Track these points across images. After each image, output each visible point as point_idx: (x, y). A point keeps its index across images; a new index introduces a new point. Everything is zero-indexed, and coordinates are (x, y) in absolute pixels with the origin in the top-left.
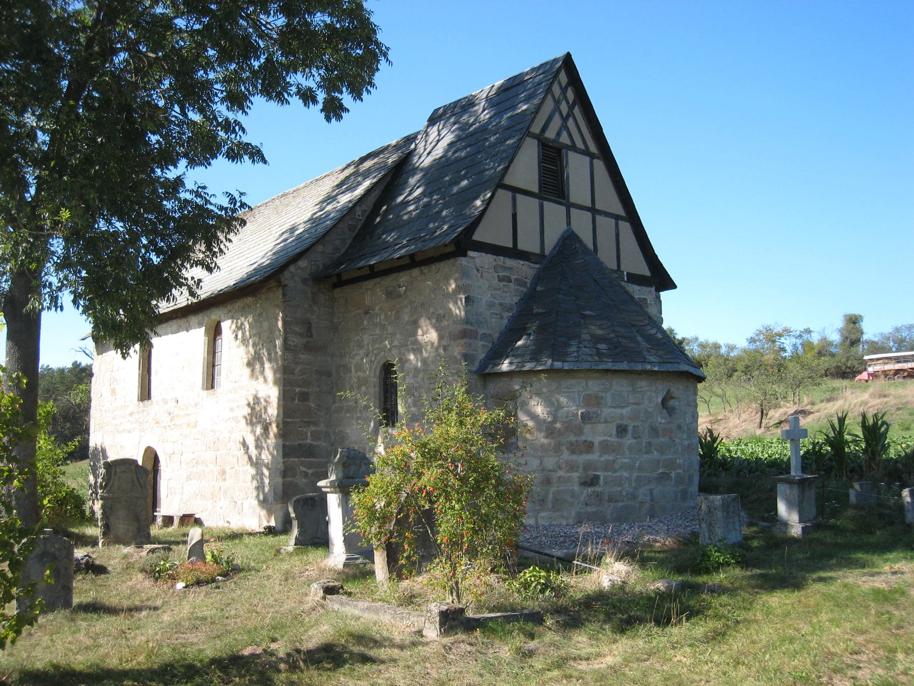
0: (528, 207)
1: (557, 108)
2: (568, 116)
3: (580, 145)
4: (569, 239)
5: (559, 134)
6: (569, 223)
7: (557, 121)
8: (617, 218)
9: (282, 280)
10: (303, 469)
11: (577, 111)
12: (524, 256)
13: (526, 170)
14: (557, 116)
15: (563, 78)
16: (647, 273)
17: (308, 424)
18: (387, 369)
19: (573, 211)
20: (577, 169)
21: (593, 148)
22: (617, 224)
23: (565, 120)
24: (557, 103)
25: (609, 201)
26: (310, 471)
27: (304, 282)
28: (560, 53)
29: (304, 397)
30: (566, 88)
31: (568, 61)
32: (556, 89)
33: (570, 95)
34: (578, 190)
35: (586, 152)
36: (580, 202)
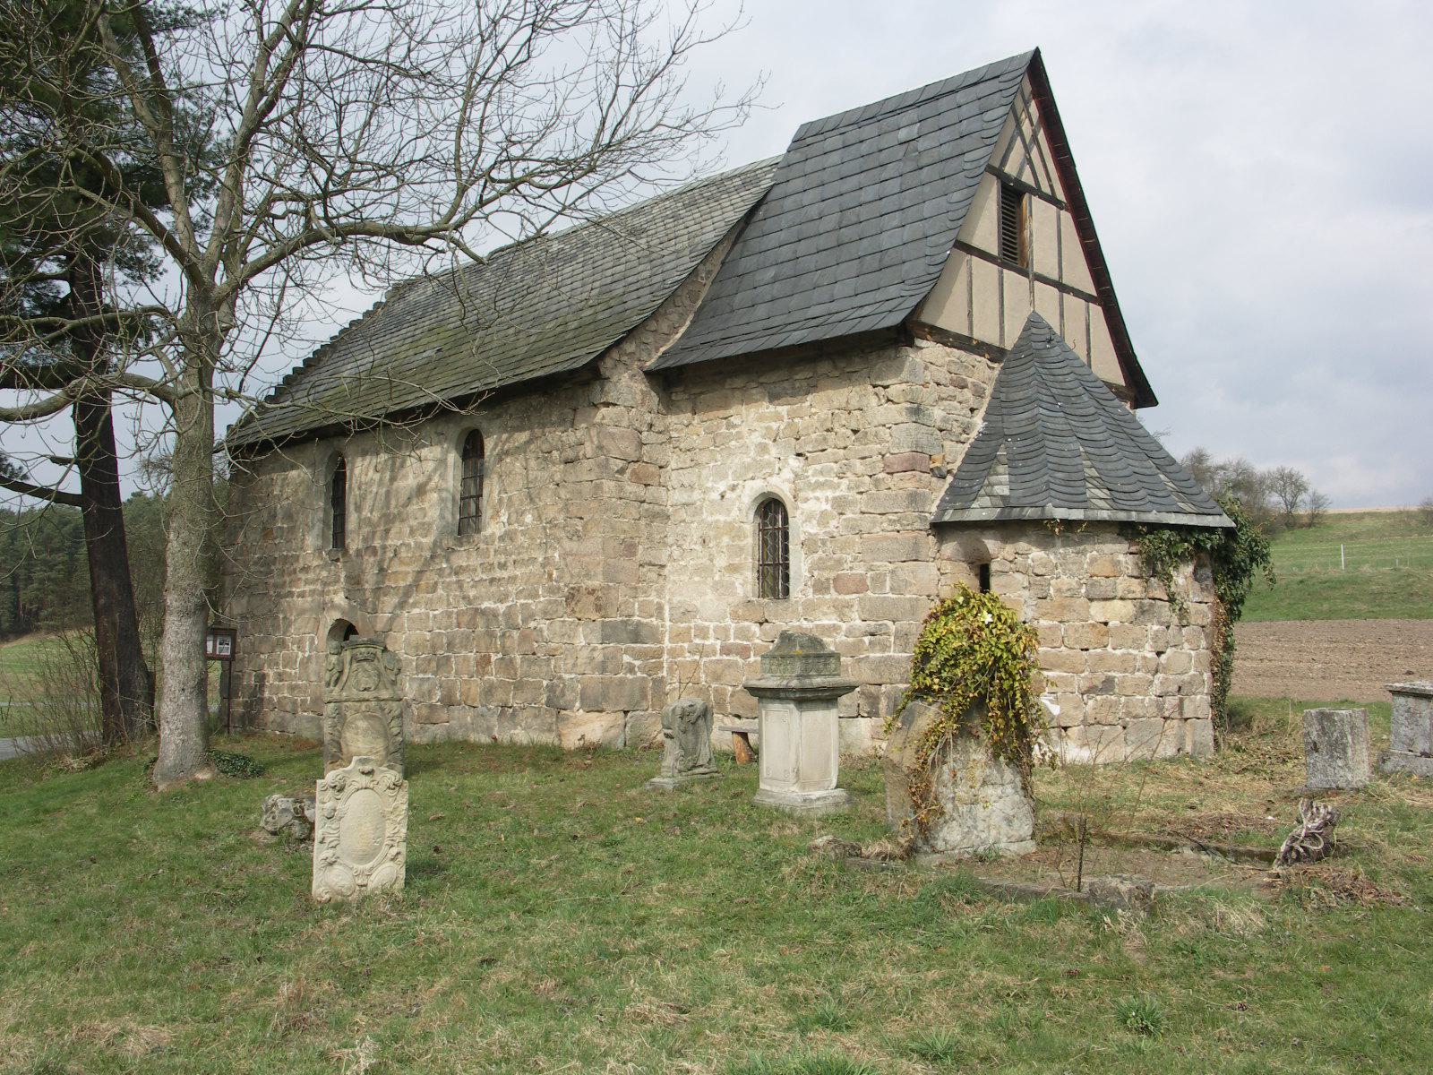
3: (1046, 189)
4: (1034, 323)
5: (1021, 171)
6: (1032, 302)
9: (602, 370)
10: (626, 658)
11: (1041, 136)
12: (980, 348)
14: (1019, 141)
18: (770, 507)
20: (1044, 224)
21: (1061, 195)
22: (1061, 277)
26: (637, 663)
28: (1024, 48)
31: (1035, 67)
34: (1042, 256)
35: (1052, 199)
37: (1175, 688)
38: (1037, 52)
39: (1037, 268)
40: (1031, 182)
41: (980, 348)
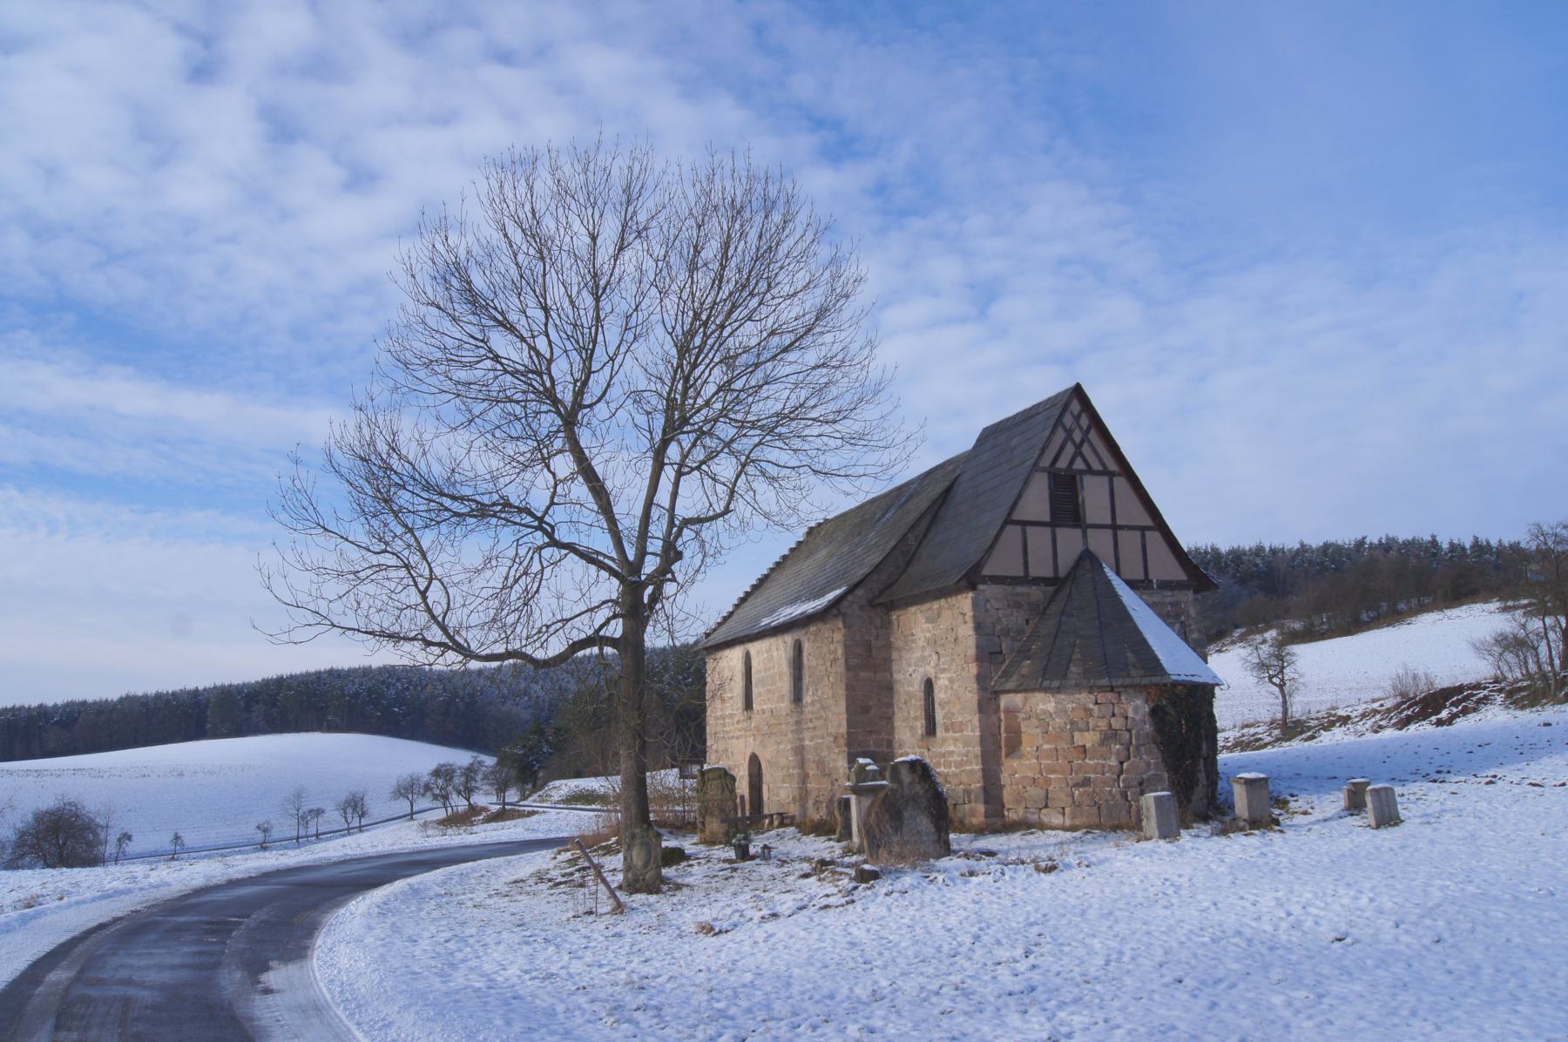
0: (1039, 540)
1: (1069, 432)
2: (1082, 441)
3: (1096, 466)
5: (1072, 462)
7: (1070, 449)
8: (1143, 529)
13: (1037, 503)
15: (1075, 406)
16: (1182, 576)
17: (871, 732)
19: (1089, 531)
20: (1094, 496)
23: (1078, 447)
24: (1069, 432)
25: (1130, 511)
27: (862, 608)
29: (866, 710)
30: (1079, 416)
31: (1078, 392)
32: (1068, 420)
33: (1085, 421)
35: (1105, 472)
36: (1098, 522)
39: (1089, 521)
41: (1037, 581)
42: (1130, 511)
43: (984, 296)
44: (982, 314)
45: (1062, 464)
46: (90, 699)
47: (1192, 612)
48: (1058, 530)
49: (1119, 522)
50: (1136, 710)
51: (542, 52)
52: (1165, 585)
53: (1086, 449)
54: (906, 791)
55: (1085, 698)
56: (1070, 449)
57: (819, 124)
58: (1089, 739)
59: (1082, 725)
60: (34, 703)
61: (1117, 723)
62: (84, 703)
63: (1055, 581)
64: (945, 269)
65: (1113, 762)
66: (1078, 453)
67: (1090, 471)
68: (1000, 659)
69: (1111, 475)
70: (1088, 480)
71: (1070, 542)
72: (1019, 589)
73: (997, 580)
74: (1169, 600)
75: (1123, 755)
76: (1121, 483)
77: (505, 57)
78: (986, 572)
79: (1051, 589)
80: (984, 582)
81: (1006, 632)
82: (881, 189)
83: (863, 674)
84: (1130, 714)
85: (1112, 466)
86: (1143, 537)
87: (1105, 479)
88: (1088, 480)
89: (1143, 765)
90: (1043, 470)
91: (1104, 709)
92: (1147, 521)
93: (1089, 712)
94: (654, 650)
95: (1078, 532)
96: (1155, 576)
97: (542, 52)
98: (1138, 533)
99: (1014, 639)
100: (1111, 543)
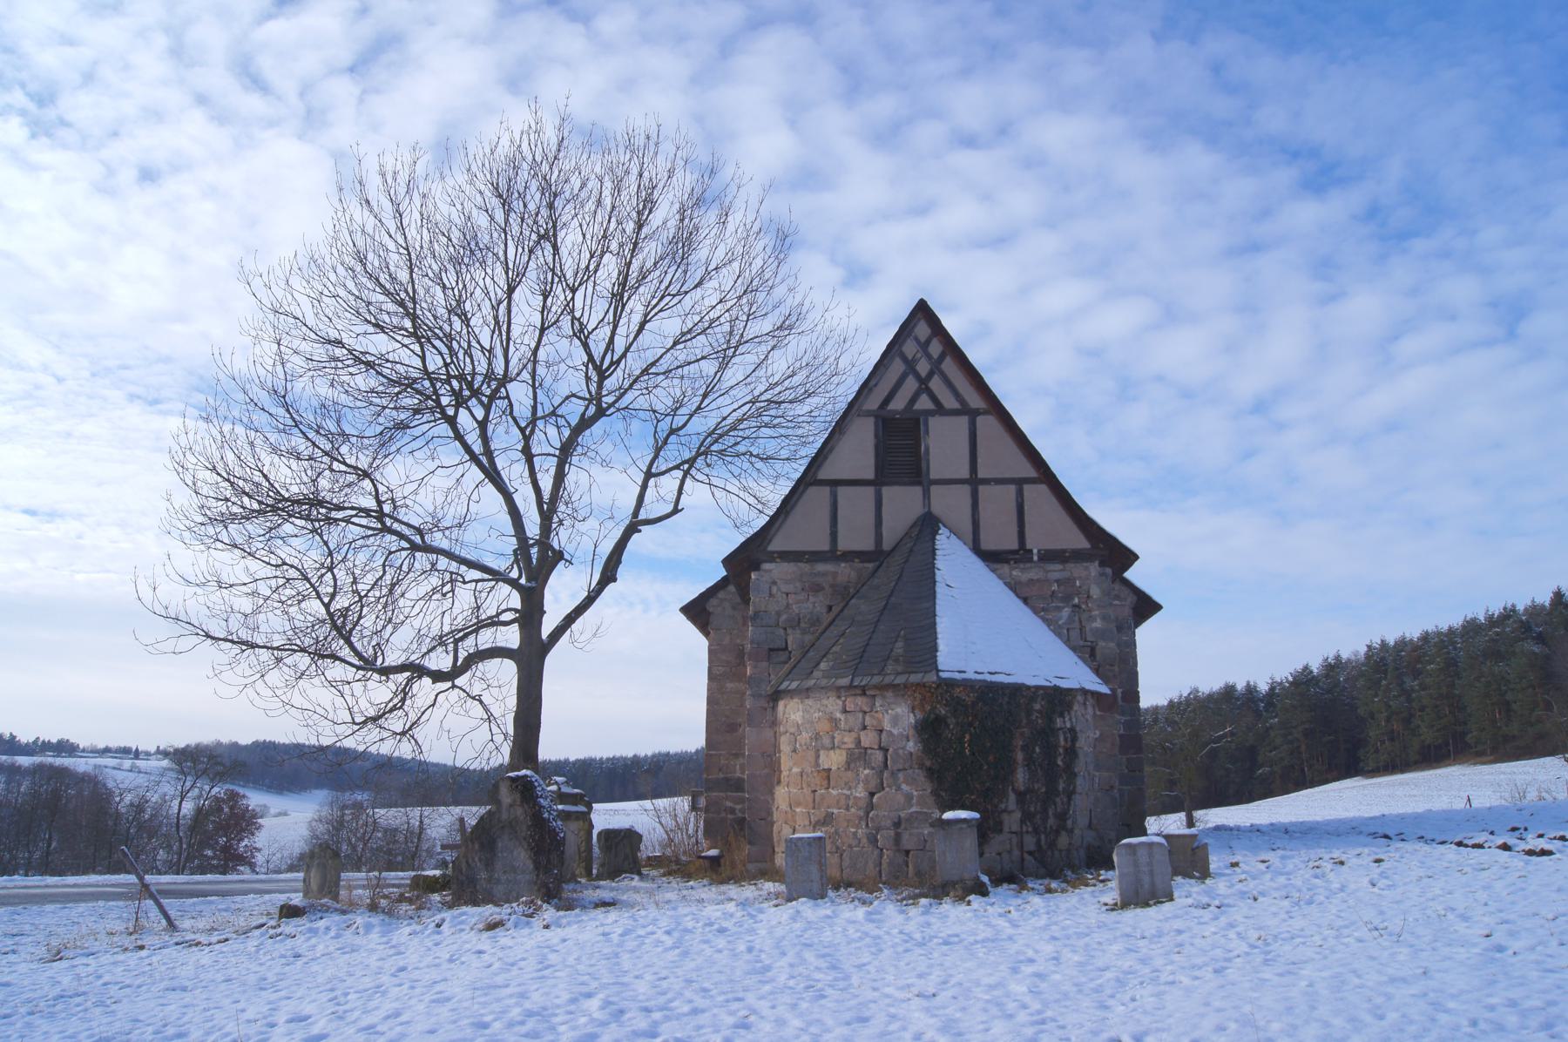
2: (930, 375)
3: (950, 402)
5: (913, 400)
8: (1020, 482)
15: (923, 330)
19: (933, 489)
20: (944, 445)
24: (910, 365)
30: (928, 342)
33: (936, 348)
35: (965, 410)
37: (889, 823)
38: (922, 311)
39: (933, 476)
40: (929, 405)
41: (849, 556)
42: (999, 459)
43: (1510, 315)
44: (1511, 335)
45: (898, 404)
46: (672, 751)
47: (1095, 592)
48: (886, 491)
49: (981, 475)
50: (895, 720)
51: (1004, 131)
52: (1049, 556)
53: (936, 384)
54: (505, 816)
55: (833, 704)
56: (911, 384)
57: (1294, 155)
58: (833, 760)
59: (826, 741)
60: (630, 755)
61: (868, 739)
62: (668, 754)
63: (877, 556)
64: (1462, 290)
65: (860, 792)
66: (924, 386)
67: (940, 410)
68: (783, 656)
69: (973, 414)
70: (935, 423)
71: (902, 504)
72: (821, 567)
73: (785, 556)
74: (1057, 575)
75: (873, 783)
76: (987, 424)
77: (968, 141)
78: (776, 545)
79: (870, 566)
80: (772, 560)
81: (795, 622)
82: (1373, 213)
83: (729, 685)
84: (887, 726)
85: (975, 401)
86: (1020, 493)
87: (964, 421)
88: (935, 423)
89: (900, 798)
90: (868, 414)
91: (851, 718)
92: (1029, 471)
93: (834, 722)
94: (1155, 710)
95: (918, 490)
96: (1035, 544)
97: (1004, 131)
98: (1012, 488)
99: (804, 632)
100: (968, 501)
